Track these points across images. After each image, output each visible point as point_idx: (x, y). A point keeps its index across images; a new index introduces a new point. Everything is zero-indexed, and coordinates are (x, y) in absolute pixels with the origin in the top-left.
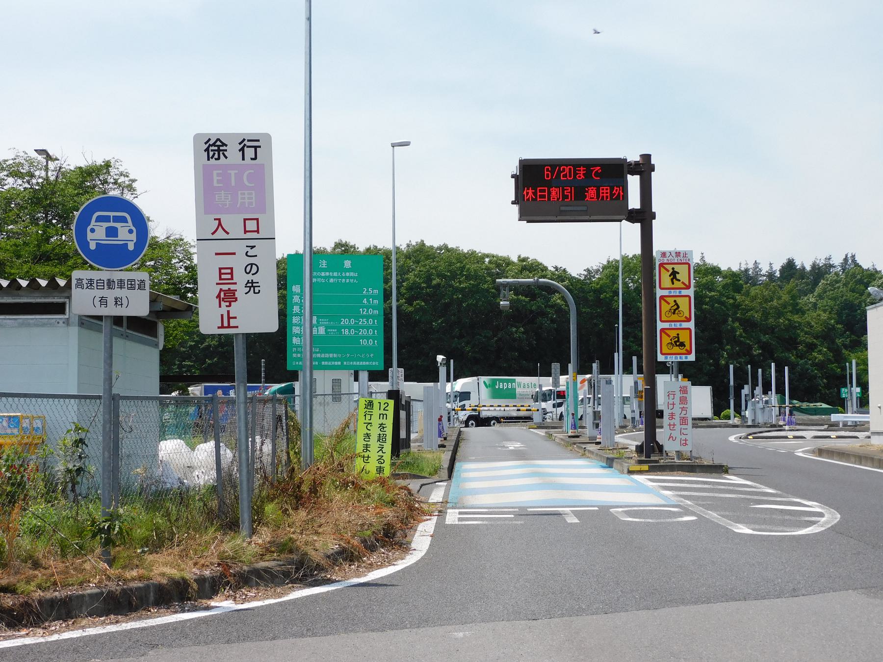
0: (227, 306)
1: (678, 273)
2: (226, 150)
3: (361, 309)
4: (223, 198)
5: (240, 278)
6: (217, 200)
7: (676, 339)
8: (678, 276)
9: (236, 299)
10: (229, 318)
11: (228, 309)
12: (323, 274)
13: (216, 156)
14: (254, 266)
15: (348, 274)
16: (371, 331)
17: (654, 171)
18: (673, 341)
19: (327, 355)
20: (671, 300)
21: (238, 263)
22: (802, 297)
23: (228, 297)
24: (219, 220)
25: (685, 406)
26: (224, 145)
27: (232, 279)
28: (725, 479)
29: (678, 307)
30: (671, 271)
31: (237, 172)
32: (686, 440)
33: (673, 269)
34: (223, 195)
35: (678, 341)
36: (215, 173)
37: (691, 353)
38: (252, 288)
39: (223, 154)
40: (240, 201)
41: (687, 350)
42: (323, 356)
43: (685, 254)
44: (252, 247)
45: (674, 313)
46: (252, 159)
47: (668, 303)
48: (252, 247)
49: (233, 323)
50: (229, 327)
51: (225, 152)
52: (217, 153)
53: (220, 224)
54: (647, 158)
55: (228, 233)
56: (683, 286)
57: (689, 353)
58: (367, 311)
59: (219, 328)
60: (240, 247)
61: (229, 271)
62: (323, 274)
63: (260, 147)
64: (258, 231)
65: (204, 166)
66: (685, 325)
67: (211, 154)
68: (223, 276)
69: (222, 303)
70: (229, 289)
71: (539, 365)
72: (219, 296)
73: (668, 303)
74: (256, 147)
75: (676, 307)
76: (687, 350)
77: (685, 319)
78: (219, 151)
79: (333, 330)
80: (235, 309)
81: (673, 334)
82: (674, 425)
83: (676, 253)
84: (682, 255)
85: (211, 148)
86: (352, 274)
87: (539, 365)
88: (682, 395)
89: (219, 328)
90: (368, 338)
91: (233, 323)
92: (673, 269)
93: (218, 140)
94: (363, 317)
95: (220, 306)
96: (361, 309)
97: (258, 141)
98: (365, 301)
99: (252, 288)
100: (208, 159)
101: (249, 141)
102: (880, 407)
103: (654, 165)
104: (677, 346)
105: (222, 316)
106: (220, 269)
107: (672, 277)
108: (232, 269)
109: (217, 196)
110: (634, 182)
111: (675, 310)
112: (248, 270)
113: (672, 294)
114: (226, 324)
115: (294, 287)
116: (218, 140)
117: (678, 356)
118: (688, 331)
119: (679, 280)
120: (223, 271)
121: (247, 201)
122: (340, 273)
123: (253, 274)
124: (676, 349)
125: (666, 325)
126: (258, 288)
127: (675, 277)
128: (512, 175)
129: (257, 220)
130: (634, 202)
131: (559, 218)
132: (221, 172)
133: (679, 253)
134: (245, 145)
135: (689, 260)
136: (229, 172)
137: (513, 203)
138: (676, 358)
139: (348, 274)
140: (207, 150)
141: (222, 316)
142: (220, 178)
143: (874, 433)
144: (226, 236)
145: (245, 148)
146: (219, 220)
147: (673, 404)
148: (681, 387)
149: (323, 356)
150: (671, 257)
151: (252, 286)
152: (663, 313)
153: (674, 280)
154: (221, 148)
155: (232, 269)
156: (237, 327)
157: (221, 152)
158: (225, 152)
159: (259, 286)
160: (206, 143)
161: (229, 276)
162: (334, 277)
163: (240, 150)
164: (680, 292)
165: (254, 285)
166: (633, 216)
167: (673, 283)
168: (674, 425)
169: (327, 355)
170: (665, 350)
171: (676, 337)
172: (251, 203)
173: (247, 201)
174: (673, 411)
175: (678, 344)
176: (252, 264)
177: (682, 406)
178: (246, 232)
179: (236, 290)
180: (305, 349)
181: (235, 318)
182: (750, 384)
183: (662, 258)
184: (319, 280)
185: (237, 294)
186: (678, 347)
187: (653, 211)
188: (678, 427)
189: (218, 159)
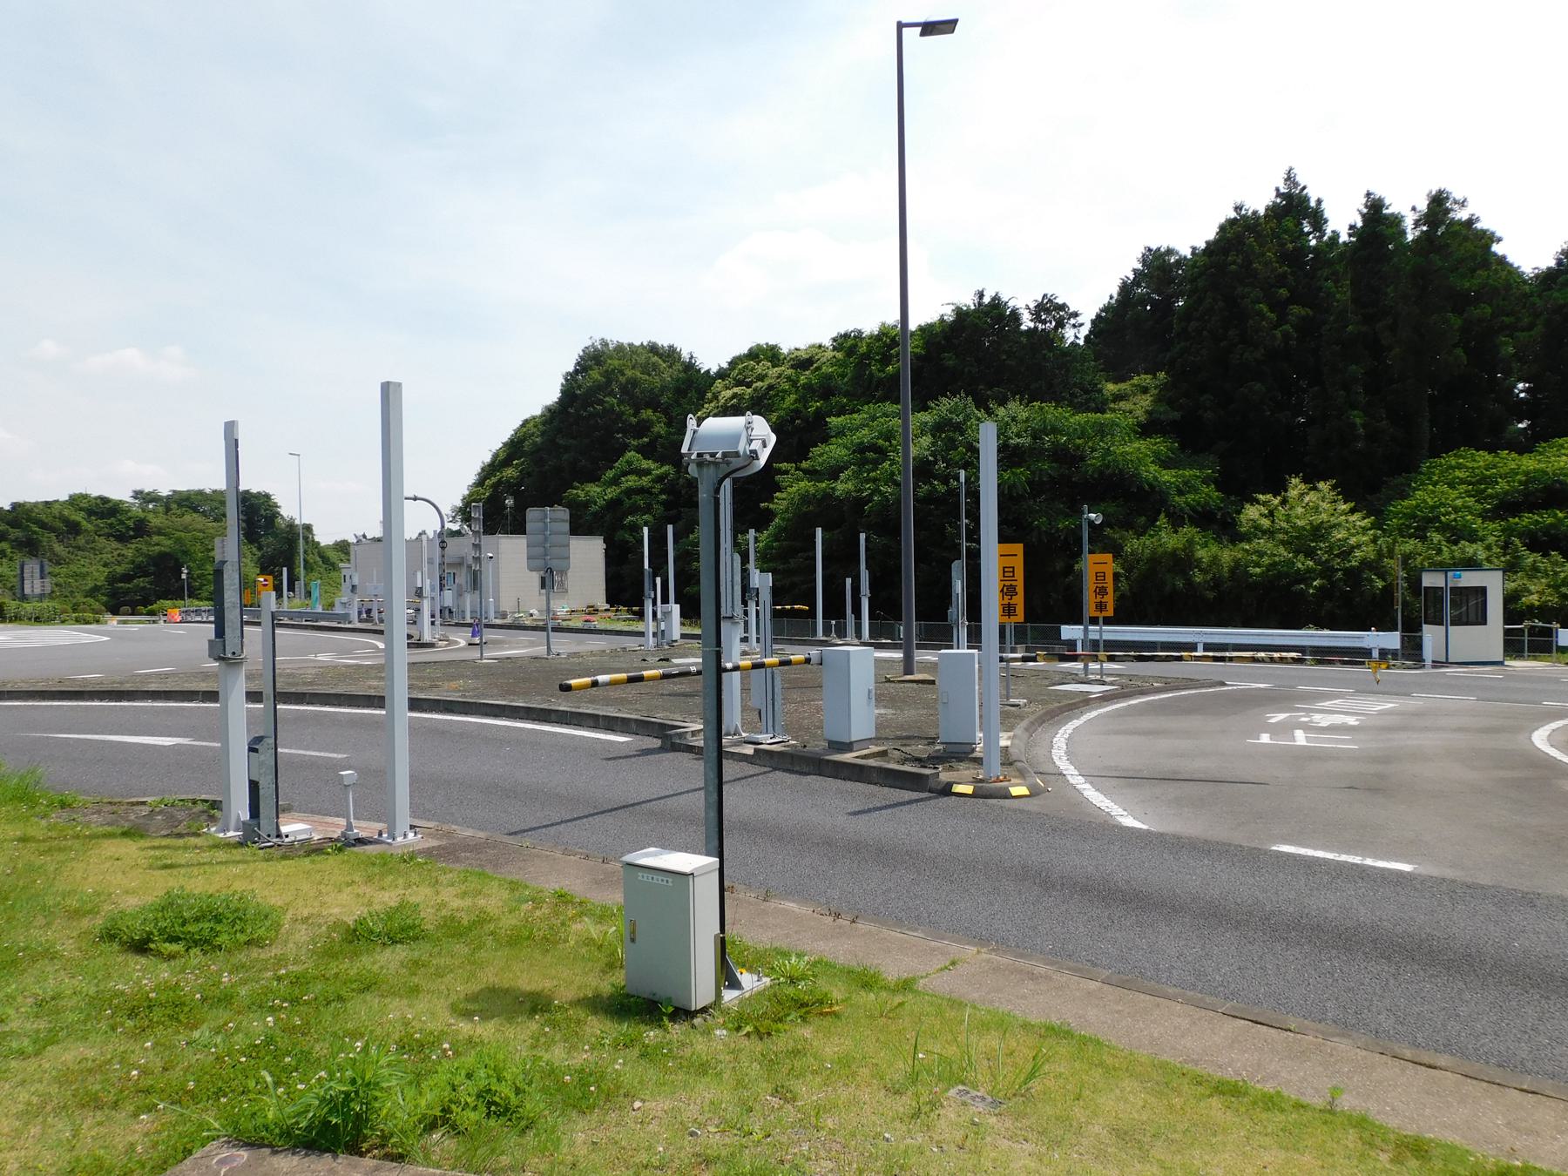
9: (1017, 593)
22: (159, 966)
27: (1013, 576)
61: (1011, 570)
68: (1006, 574)
71: (777, 607)
87: (780, 607)
106: (1004, 568)
120: (1006, 570)
155: (1013, 568)
161: (1011, 574)
187: (679, 605)
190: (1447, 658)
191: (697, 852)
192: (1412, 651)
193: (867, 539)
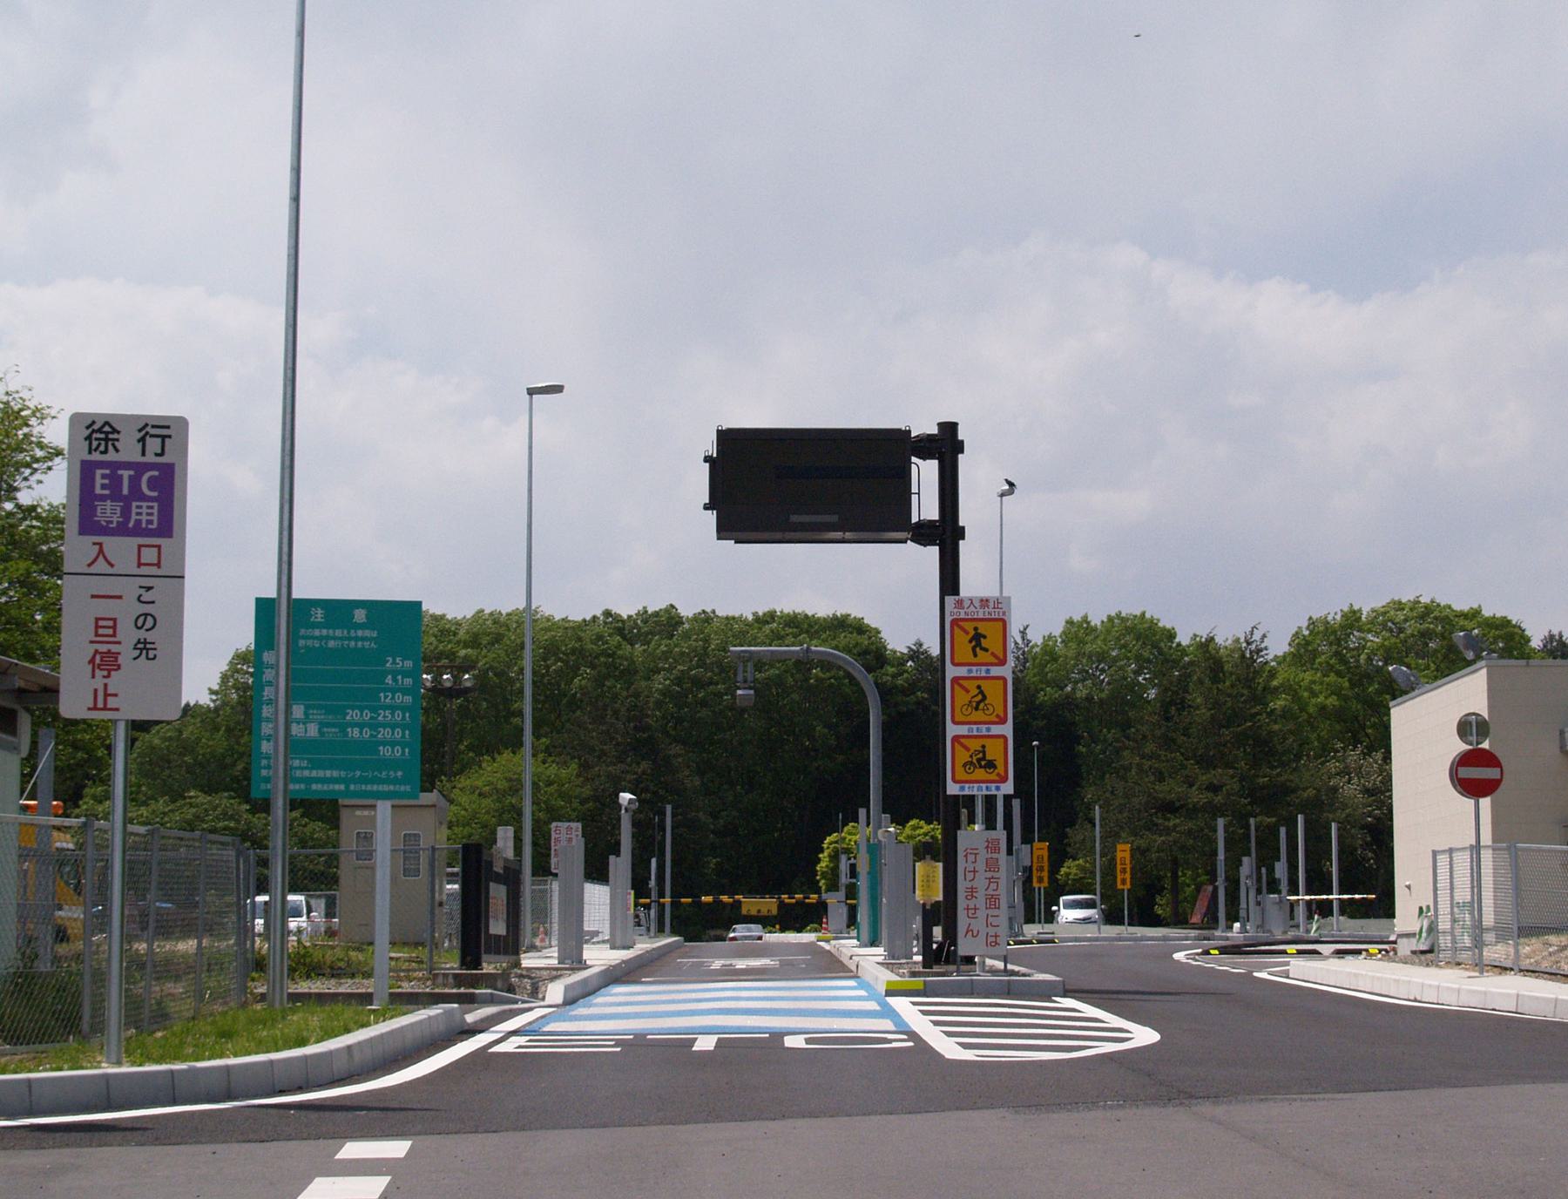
0: (104, 677)
1: (985, 637)
2: (117, 440)
3: (382, 695)
4: (109, 511)
5: (128, 635)
6: (118, 508)
7: (981, 755)
8: (984, 643)
9: (119, 667)
10: (106, 695)
11: (106, 681)
12: (317, 632)
13: (102, 448)
14: (149, 618)
15: (360, 633)
16: (398, 733)
17: (962, 452)
18: (975, 758)
19: (321, 773)
20: (971, 685)
21: (125, 612)
23: (106, 663)
24: (100, 544)
25: (996, 875)
26: (115, 431)
27: (114, 635)
28: (1055, 1002)
29: (984, 698)
30: (972, 633)
31: (132, 473)
32: (996, 936)
33: (976, 629)
34: (108, 508)
35: (984, 758)
36: (99, 472)
37: (1007, 779)
38: (144, 652)
39: (113, 445)
40: (134, 517)
41: (998, 774)
42: (314, 774)
43: (998, 602)
44: (149, 589)
45: (977, 709)
46: (157, 455)
47: (967, 691)
48: (149, 589)
49: (112, 702)
50: (105, 708)
51: (116, 443)
52: (103, 443)
53: (101, 551)
54: (949, 429)
55: (112, 565)
56: (994, 660)
57: (1004, 779)
58: (393, 698)
59: (89, 709)
60: (130, 588)
61: (110, 623)
62: (317, 632)
63: (170, 437)
64: (158, 565)
65: (83, 463)
66: (996, 730)
67: (95, 443)
68: (101, 631)
69: (97, 671)
70: (109, 652)
72: (92, 661)
73: (967, 691)
74: (164, 437)
75: (980, 697)
76: (998, 774)
77: (997, 720)
78: (107, 440)
79: (333, 730)
80: (116, 679)
81: (975, 745)
82: (975, 909)
83: (982, 600)
84: (991, 605)
85: (95, 436)
86: (367, 633)
88: (990, 856)
89: (89, 709)
90: (393, 744)
91: (112, 702)
92: (976, 629)
93: (107, 423)
94: (385, 708)
95: (93, 677)
96: (382, 695)
97: (168, 427)
98: (389, 680)
99: (144, 652)
100: (90, 453)
101: (153, 427)
102: (1409, 887)
103: (962, 442)
104: (981, 767)
105: (96, 691)
106: (97, 619)
107: (974, 643)
108: (115, 620)
109: (99, 508)
110: (926, 473)
111: (978, 703)
112: (140, 623)
113: (974, 674)
114: (100, 705)
115: (266, 654)
116: (107, 423)
117: (984, 785)
118: (1002, 740)
119: (986, 650)
120: (101, 623)
121: (144, 518)
122: (345, 632)
123: (147, 630)
124: (980, 774)
125: (963, 730)
126: (155, 652)
127: (979, 644)
128: (706, 457)
129: (159, 547)
130: (926, 506)
131: (788, 535)
132: (107, 472)
133: (987, 600)
134: (147, 433)
135: (1004, 613)
136: (120, 472)
137: (706, 507)
138: (980, 789)
139: (360, 633)
140: (89, 438)
141: (96, 691)
142: (106, 481)
143: (1400, 936)
144: (111, 571)
145: (148, 437)
146: (100, 544)
147: (974, 871)
148: (987, 841)
149: (314, 774)
150: (972, 608)
151: (145, 648)
152: (957, 710)
153: (978, 649)
154: (111, 436)
155: (115, 620)
156: (117, 709)
157: (110, 443)
158: (116, 443)
159: (155, 649)
160: (88, 428)
161: (110, 631)
162: (335, 638)
163: (139, 441)
164: (988, 671)
165: (148, 646)
166: (923, 534)
167: (975, 655)
168: (975, 909)
169: (321, 773)
170: (961, 775)
171: (980, 752)
172: (150, 522)
173: (144, 518)
174: (975, 884)
175: (983, 763)
176: (146, 615)
177: (989, 875)
178: (140, 565)
179: (119, 653)
180: (277, 760)
181: (116, 695)
182: (1254, 855)
183: (956, 610)
184: (310, 643)
185: (121, 660)
186: (983, 770)
188: (982, 914)
189: (105, 452)
190: (110, 695)
191: (360, 615)
192: (1528, 665)
193: (1226, 828)
